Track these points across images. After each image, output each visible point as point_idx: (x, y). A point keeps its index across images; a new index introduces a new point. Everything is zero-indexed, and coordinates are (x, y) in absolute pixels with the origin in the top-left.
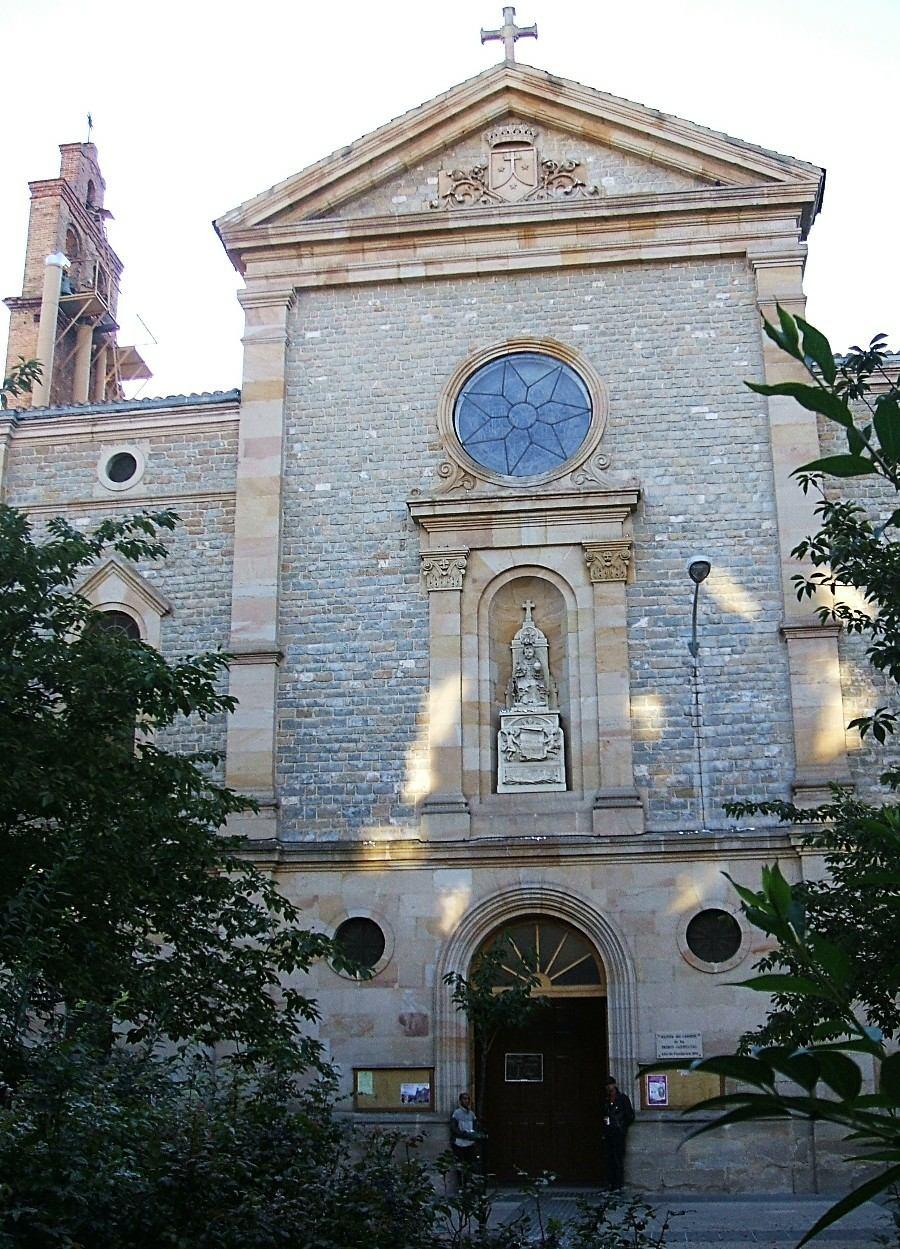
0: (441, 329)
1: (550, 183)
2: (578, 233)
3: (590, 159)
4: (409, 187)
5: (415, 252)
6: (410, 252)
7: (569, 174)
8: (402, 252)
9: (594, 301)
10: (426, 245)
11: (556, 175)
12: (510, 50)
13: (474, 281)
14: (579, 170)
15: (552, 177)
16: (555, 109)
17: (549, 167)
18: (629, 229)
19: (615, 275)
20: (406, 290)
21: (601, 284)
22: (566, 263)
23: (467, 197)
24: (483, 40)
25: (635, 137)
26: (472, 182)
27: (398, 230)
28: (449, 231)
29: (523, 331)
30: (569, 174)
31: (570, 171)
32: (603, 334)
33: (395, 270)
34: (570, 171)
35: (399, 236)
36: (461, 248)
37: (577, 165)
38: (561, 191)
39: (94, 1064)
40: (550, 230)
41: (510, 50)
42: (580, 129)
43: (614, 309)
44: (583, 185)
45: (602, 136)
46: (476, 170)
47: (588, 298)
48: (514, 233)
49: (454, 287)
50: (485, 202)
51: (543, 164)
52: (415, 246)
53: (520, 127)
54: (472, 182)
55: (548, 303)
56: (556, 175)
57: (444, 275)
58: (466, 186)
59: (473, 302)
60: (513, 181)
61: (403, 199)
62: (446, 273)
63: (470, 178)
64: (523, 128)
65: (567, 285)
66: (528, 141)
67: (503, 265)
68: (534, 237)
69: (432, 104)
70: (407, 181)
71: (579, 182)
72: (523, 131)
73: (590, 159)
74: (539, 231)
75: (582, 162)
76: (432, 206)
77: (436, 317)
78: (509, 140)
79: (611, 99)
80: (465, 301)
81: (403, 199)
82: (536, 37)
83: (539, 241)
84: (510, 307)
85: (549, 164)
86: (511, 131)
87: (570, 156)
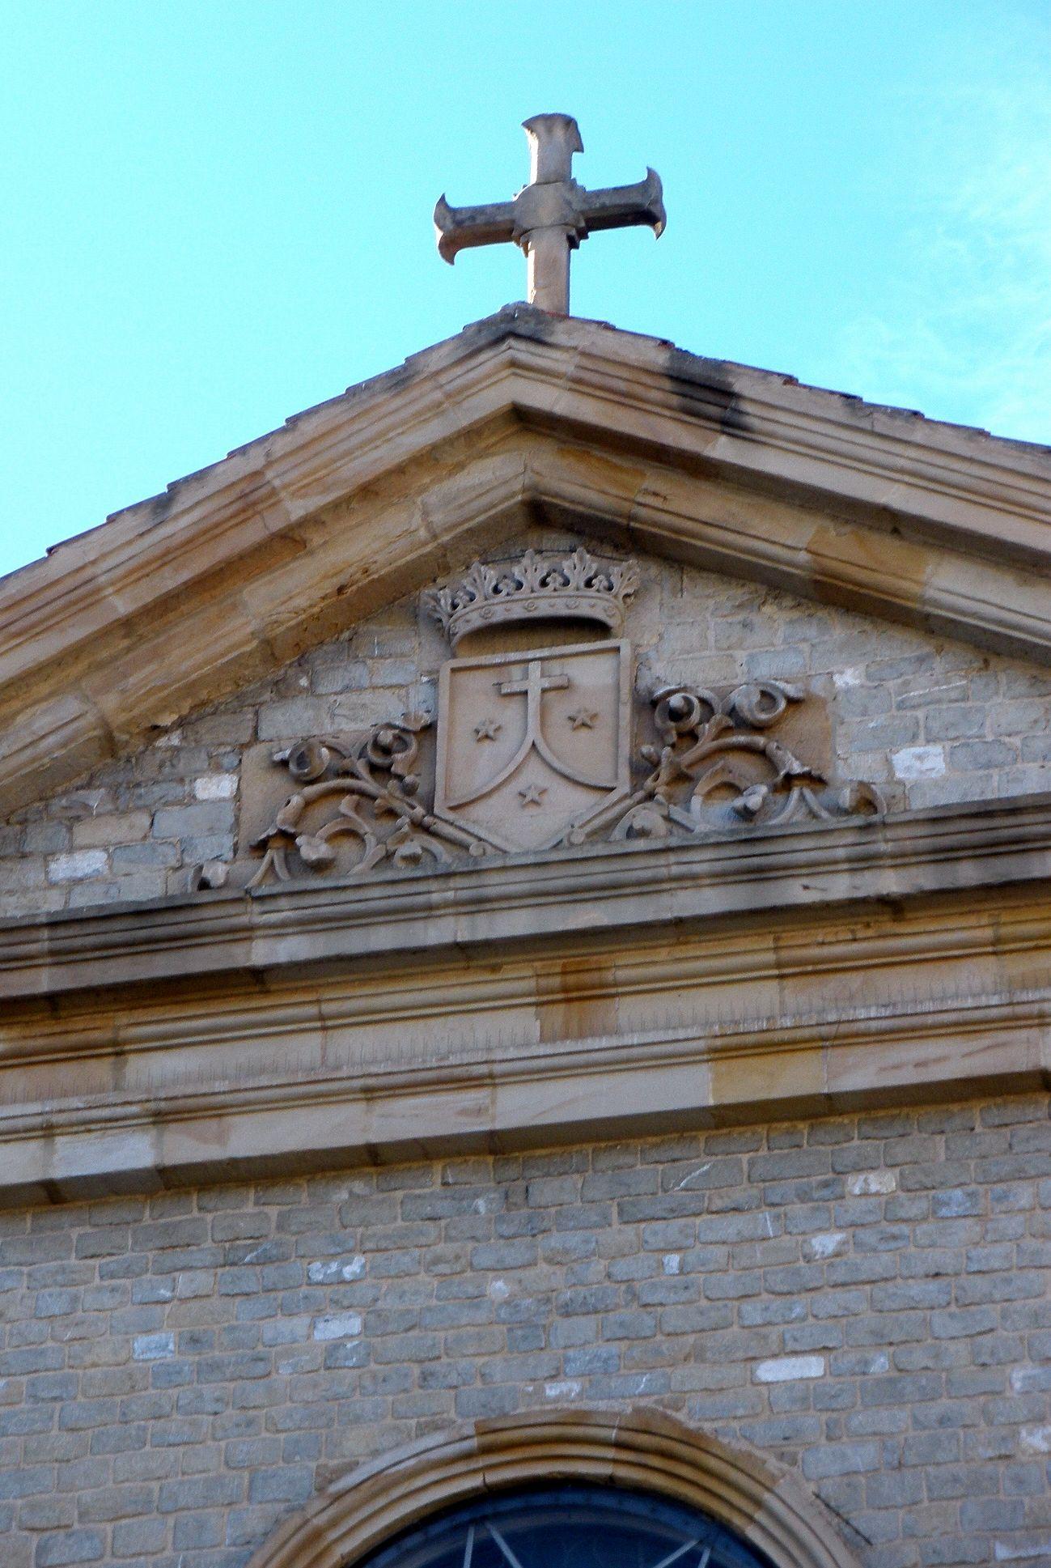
0: (209, 1390)
1: (682, 777)
2: (784, 972)
3: (848, 678)
4: (123, 813)
5: (119, 1069)
6: (100, 1070)
7: (760, 740)
8: (67, 1073)
9: (852, 1255)
10: (165, 1044)
11: (705, 744)
12: (554, 276)
13: (359, 1187)
14: (804, 723)
15: (689, 756)
16: (705, 486)
17: (676, 715)
18: (997, 948)
19: (940, 1140)
20: (74, 1229)
21: (882, 1182)
22: (731, 1098)
23: (348, 847)
24: (449, 248)
25: (1025, 582)
26: (368, 784)
27: (44, 981)
28: (258, 979)
29: (552, 1390)
30: (760, 740)
31: (759, 728)
32: (889, 1391)
33: (34, 1147)
34: (759, 728)
35: (54, 1003)
36: (305, 1050)
37: (793, 702)
38: (727, 805)
39: (925, 1140)
40: (663, 961)
41: (554, 276)
42: (803, 557)
43: (933, 1286)
44: (815, 781)
45: (906, 585)
46: (387, 737)
47: (826, 1243)
48: (519, 978)
49: (273, 1211)
50: (413, 859)
51: (654, 703)
52: (119, 1050)
53: (566, 565)
54: (368, 784)
55: (661, 1264)
56: (705, 744)
57: (234, 1162)
58: (345, 804)
59: (349, 1272)
60: (535, 775)
61: (91, 862)
62: (241, 1153)
63: (361, 767)
64: (578, 564)
65: (739, 1195)
66: (598, 614)
67: (479, 1111)
68: (604, 993)
69: (211, 487)
70: (115, 793)
71: (797, 768)
72: (577, 580)
73: (848, 678)
74: (626, 966)
75: (818, 687)
76: (204, 885)
77: (194, 1341)
78: (518, 612)
79: (919, 435)
80: (317, 1271)
81: (91, 862)
82: (443, 198)
83: (627, 1009)
84: (499, 1288)
85: (676, 701)
86: (531, 579)
87: (765, 670)
